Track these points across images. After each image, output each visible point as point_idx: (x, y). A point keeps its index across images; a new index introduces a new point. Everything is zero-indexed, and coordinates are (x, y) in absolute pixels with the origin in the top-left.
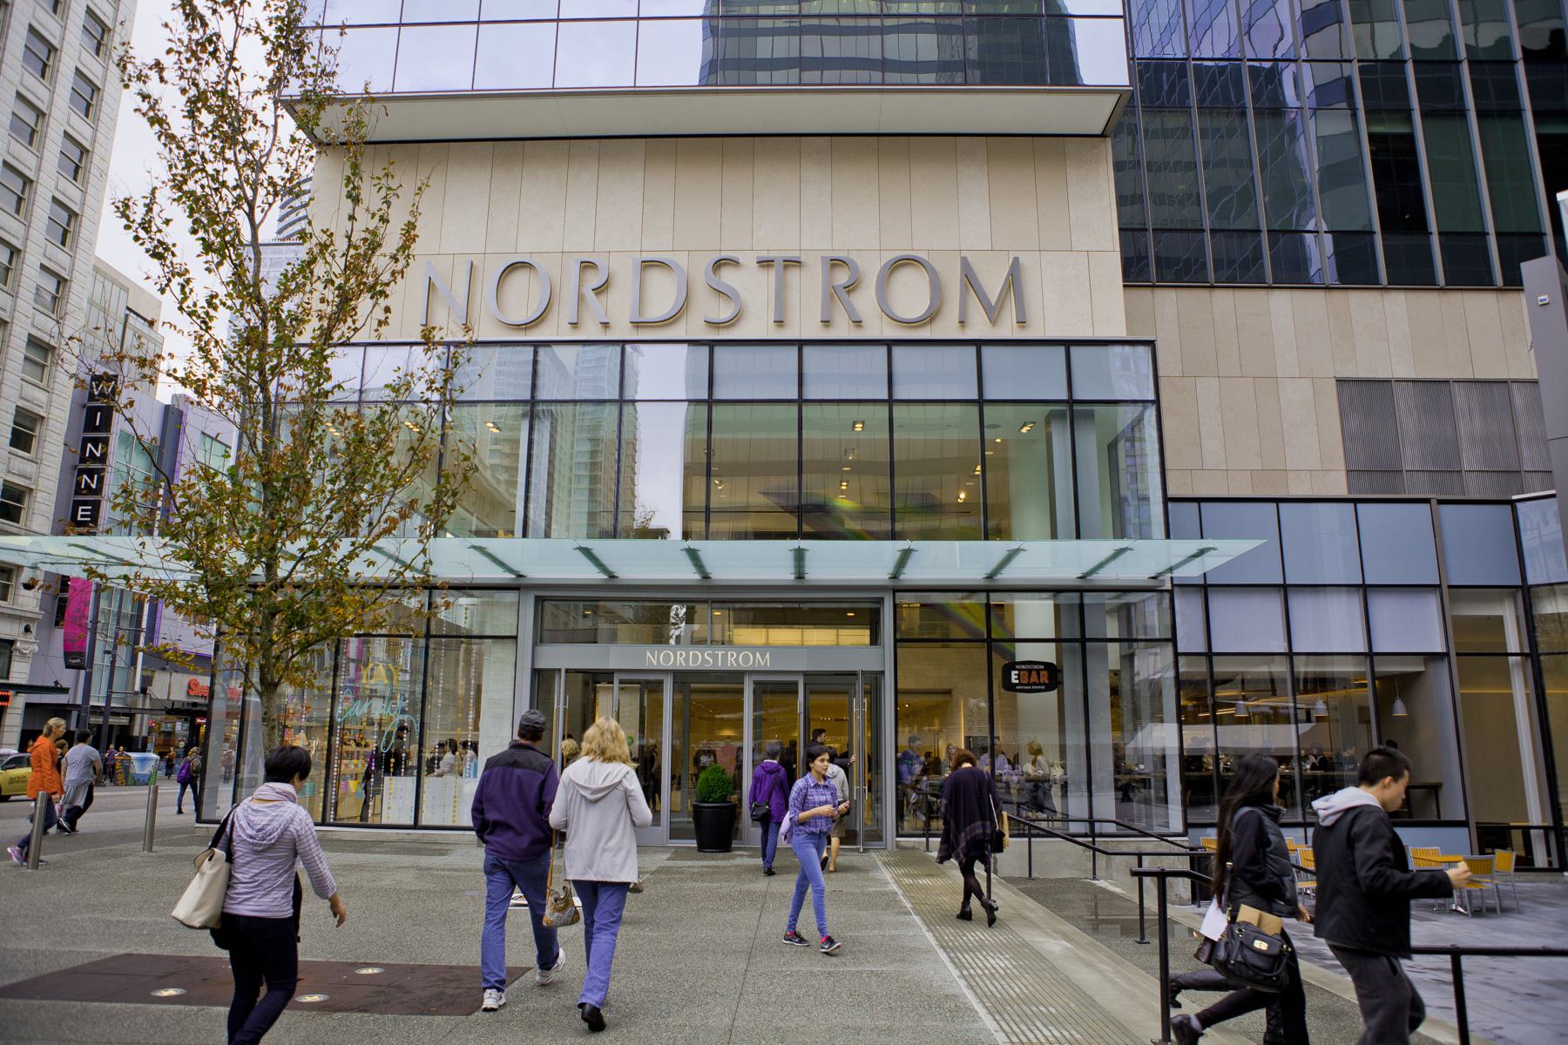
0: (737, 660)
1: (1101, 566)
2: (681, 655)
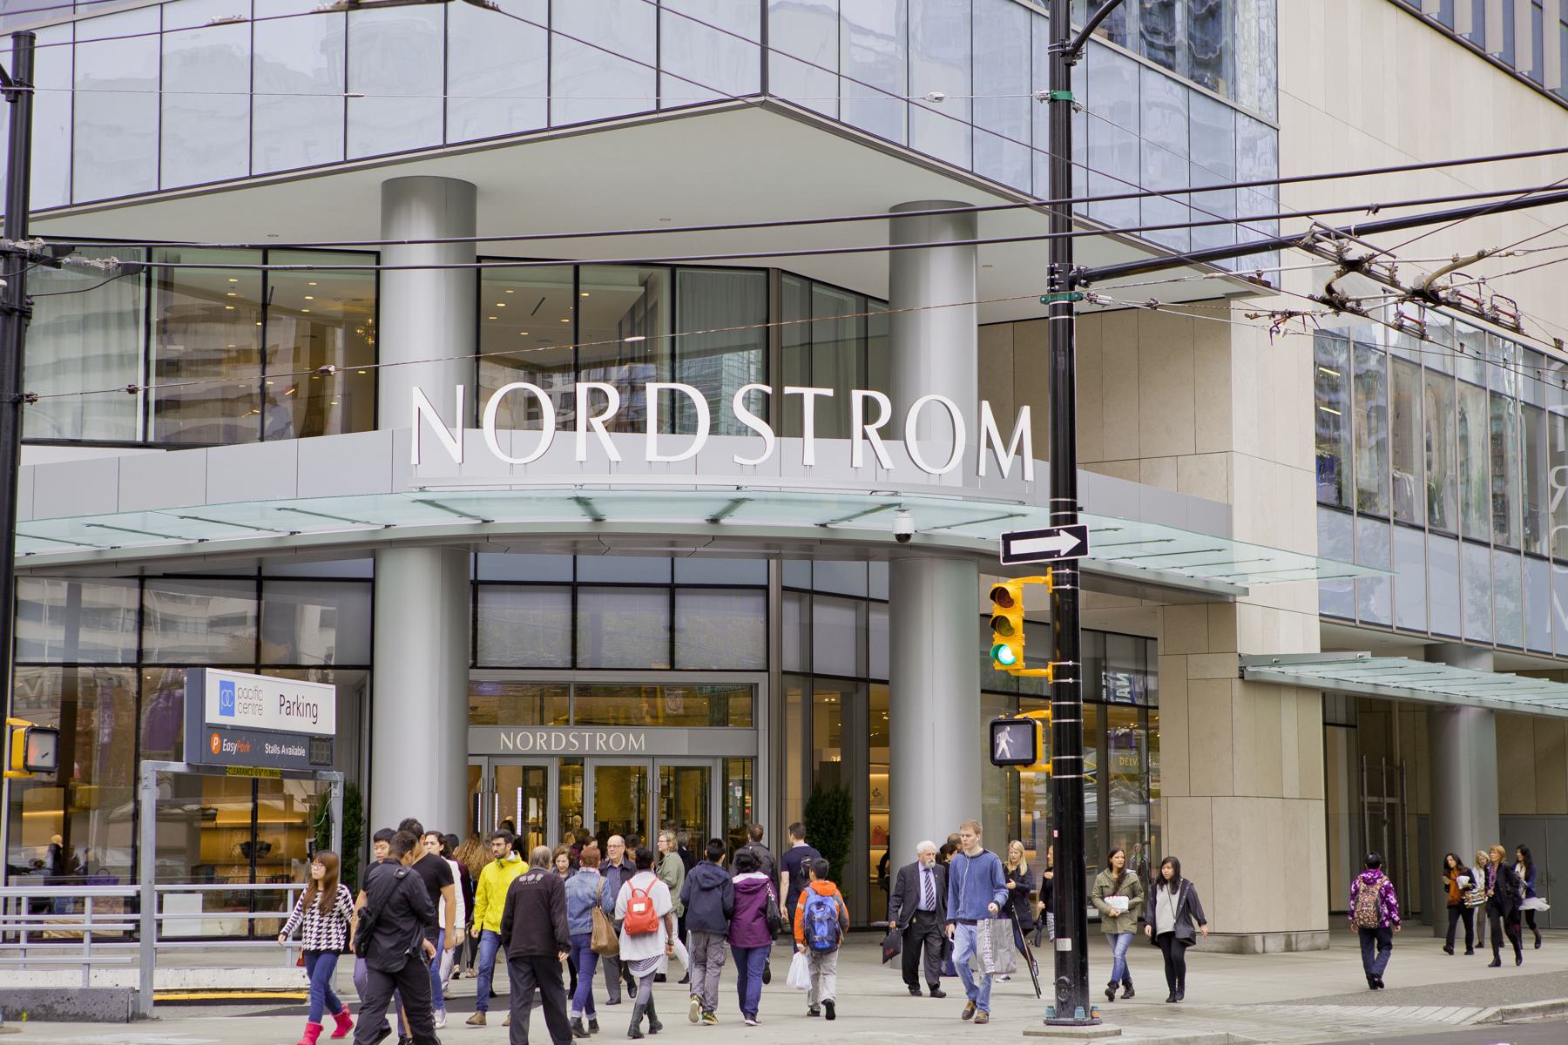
2: (542, 737)
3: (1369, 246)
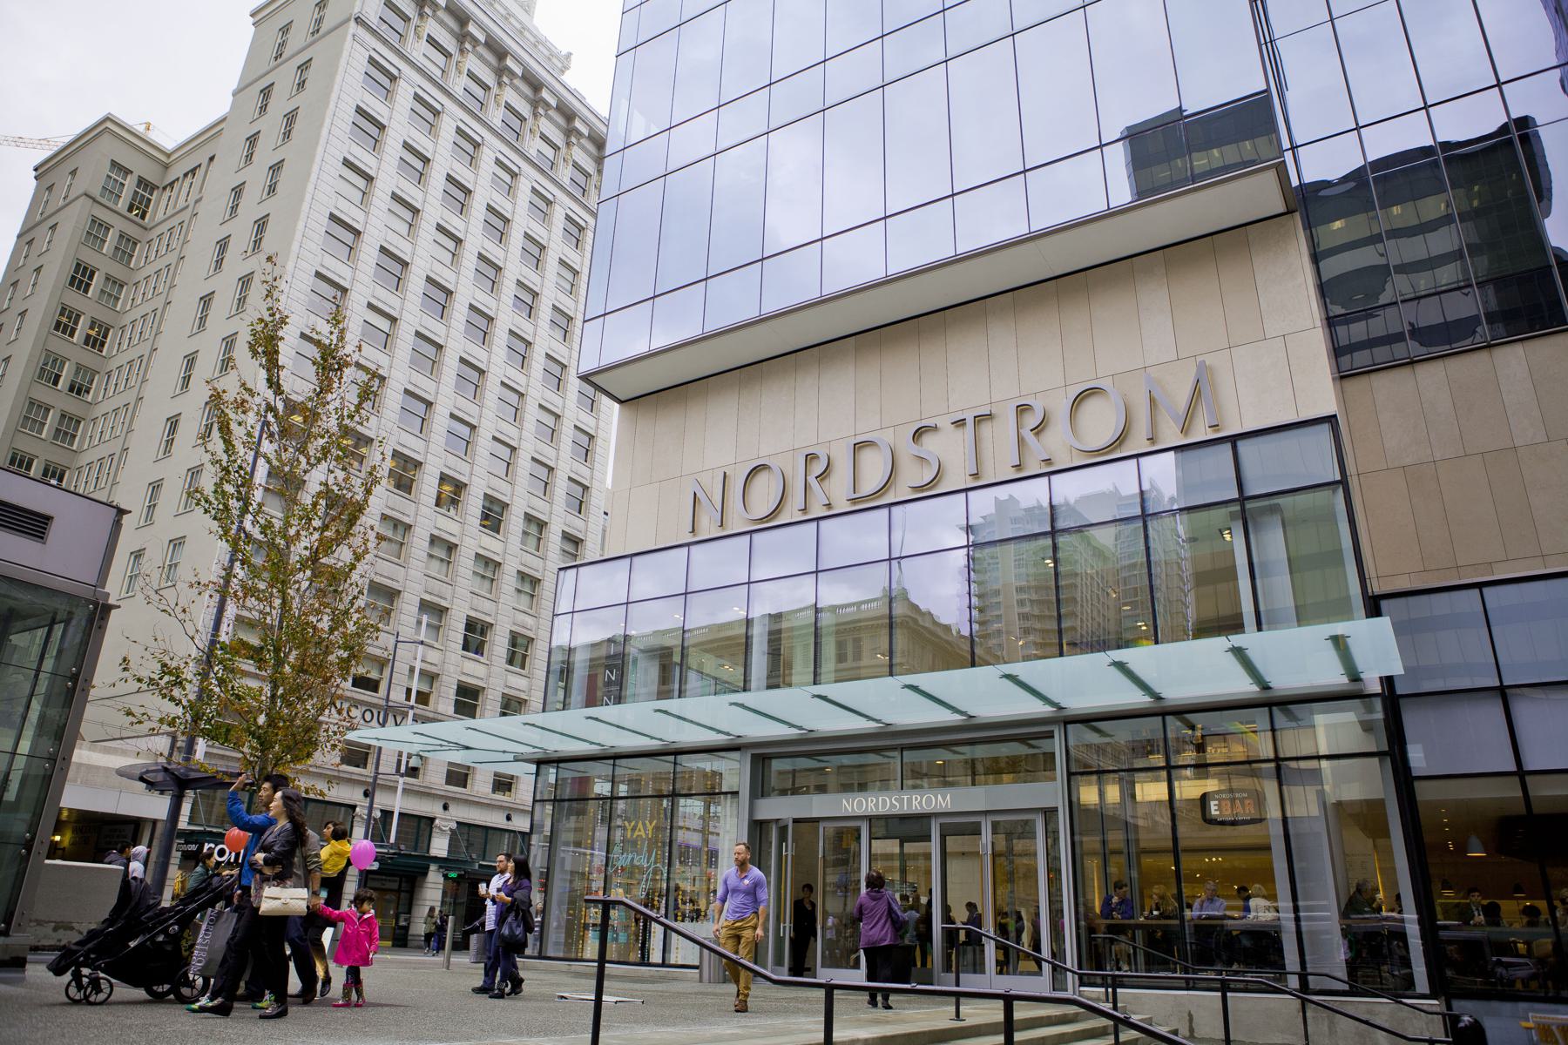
2: (872, 801)
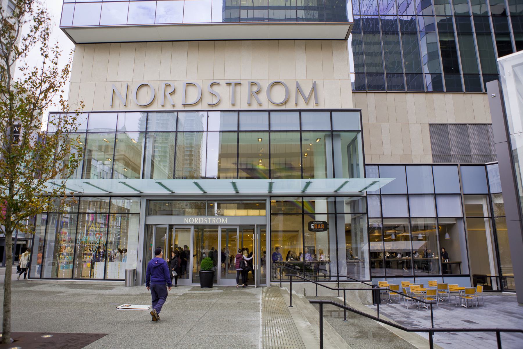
0: (215, 221)
1: (342, 186)
3: (325, 286)
